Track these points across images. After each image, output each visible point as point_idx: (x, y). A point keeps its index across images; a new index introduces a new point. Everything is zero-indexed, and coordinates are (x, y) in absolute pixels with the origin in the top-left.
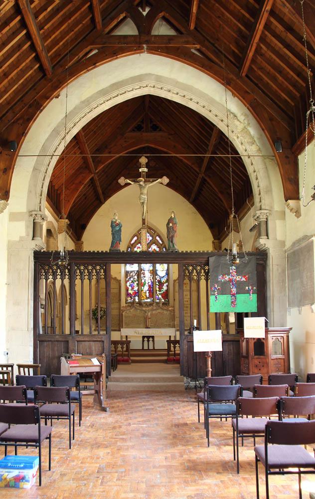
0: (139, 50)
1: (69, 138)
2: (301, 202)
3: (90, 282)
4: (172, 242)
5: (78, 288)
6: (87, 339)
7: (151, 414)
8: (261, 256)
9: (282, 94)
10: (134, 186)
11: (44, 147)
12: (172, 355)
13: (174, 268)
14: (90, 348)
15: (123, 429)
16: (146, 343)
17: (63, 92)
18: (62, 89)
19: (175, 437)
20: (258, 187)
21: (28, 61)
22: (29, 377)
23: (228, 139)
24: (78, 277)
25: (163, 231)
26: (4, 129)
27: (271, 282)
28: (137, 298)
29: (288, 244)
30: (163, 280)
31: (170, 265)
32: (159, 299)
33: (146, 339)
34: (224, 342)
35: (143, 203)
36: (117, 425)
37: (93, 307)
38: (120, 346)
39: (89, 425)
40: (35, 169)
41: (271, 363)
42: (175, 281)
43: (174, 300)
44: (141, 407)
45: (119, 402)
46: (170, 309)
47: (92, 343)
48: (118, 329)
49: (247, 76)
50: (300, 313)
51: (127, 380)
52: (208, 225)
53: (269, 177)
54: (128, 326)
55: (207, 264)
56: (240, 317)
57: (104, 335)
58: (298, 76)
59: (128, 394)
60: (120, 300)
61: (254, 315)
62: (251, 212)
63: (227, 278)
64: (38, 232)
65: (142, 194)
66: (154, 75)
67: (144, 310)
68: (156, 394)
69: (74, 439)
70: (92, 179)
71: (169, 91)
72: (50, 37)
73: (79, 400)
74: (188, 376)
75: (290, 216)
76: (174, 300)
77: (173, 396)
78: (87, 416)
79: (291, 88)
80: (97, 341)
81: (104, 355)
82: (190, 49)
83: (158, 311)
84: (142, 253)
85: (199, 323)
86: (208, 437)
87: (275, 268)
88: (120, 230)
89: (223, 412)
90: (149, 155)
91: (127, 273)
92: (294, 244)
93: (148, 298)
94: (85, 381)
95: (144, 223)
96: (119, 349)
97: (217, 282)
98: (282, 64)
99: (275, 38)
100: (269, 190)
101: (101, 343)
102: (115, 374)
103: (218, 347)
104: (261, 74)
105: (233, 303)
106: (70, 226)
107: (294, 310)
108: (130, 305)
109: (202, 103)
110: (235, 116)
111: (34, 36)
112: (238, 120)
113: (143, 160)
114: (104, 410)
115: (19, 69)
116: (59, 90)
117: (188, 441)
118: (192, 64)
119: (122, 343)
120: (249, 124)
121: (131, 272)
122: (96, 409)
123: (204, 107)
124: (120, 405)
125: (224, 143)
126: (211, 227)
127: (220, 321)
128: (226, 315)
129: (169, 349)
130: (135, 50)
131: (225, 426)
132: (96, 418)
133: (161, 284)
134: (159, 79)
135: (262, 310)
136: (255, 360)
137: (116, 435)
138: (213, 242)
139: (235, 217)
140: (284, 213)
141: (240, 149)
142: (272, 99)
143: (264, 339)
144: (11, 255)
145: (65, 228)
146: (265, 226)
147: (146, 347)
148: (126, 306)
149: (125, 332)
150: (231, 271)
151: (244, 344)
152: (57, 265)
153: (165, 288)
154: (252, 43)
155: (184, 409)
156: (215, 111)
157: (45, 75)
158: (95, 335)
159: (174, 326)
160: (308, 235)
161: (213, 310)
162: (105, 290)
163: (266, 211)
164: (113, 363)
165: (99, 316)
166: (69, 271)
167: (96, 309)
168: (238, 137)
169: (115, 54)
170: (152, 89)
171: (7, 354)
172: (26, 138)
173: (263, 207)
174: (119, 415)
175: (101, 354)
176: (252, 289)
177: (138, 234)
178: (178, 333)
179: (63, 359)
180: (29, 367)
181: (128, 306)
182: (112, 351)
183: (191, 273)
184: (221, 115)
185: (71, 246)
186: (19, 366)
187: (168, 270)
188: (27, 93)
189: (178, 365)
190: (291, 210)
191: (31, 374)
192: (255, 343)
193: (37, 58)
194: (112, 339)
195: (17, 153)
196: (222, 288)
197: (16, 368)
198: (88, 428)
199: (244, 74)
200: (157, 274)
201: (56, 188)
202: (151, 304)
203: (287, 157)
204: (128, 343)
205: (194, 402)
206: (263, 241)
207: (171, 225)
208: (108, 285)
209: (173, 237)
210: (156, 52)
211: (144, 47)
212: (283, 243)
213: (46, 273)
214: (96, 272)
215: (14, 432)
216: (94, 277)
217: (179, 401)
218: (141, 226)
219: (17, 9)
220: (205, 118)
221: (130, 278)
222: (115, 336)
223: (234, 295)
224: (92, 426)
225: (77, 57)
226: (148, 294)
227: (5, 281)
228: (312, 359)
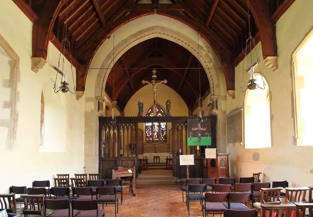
0: (152, 12)
1: (116, 60)
2: (236, 91)
3: (128, 132)
4: (169, 112)
5: (122, 134)
6: (126, 159)
7: (158, 197)
8: (213, 119)
9: (228, 35)
10: (150, 85)
11: (103, 65)
12: (169, 165)
13: (170, 124)
14: (128, 163)
15: (144, 206)
16: (155, 160)
17: (112, 35)
18: (112, 33)
19: (171, 210)
20: (213, 84)
21: (92, 17)
22: (95, 181)
23: (198, 61)
24: (122, 129)
25: (164, 106)
26: (81, 54)
27: (219, 130)
28: (151, 138)
29: (228, 112)
30: (164, 130)
31: (167, 123)
32: (162, 139)
33: (155, 158)
34: (195, 160)
35: (154, 93)
36: (141, 204)
37: (130, 143)
38: (143, 161)
39: (126, 204)
40: (98, 76)
41: (219, 171)
42: (170, 130)
43: (169, 139)
44: (153, 193)
45: (142, 191)
46: (167, 143)
47: (129, 161)
48: (142, 153)
49: (209, 26)
50: (234, 146)
51: (146, 179)
52: (186, 104)
53: (218, 79)
54: (147, 152)
55: (186, 122)
56: (203, 148)
57: (135, 157)
58: (237, 24)
59: (147, 186)
60: (143, 140)
61: (210, 147)
62: (209, 96)
63: (196, 129)
64: (101, 107)
65: (153, 88)
66: (160, 26)
67: (154, 144)
68: (161, 186)
69: (118, 213)
70: (129, 82)
71: (168, 35)
72: (104, 3)
73: (121, 191)
74: (177, 176)
75: (229, 98)
76: (169, 139)
77: (170, 187)
78: (125, 199)
79: (233, 32)
80: (131, 160)
81: (134, 167)
82: (179, 11)
83: (161, 145)
84: (154, 117)
85: (182, 151)
86: (188, 210)
87: (221, 124)
88: (143, 106)
89: (196, 198)
90: (157, 69)
91: (146, 127)
92: (231, 112)
93: (157, 138)
94: (125, 180)
95: (155, 103)
96: (143, 163)
97: (191, 131)
98: (229, 18)
99: (226, 3)
100: (218, 86)
101: (133, 161)
102: (140, 176)
103: (192, 163)
104: (218, 25)
105: (199, 141)
106: (118, 104)
107: (231, 145)
108: (148, 142)
109: (185, 41)
110: (202, 48)
111: (94, 2)
112: (203, 50)
113: (154, 71)
114: (134, 195)
115: (87, 21)
116: (109, 34)
117: (178, 213)
118: (180, 20)
119: (144, 160)
120: (209, 52)
121: (148, 126)
122: (130, 195)
123: (186, 43)
124: (143, 192)
125: (196, 62)
126: (188, 104)
127: (192, 150)
128: (195, 147)
129: (167, 163)
130: (150, 12)
131: (197, 204)
132: (130, 200)
133: (163, 132)
134: (163, 28)
135: (214, 145)
136: (211, 169)
137: (140, 210)
138: (188, 112)
139: (201, 99)
140: (226, 97)
141: (204, 65)
142: (222, 38)
143: (215, 159)
144: (87, 119)
145: (115, 105)
146: (216, 103)
147: (155, 162)
148: (146, 143)
149: (146, 155)
150: (198, 126)
151: (205, 161)
152: (111, 123)
153: (165, 133)
154: (213, 6)
155: (175, 194)
156: (191, 46)
157: (102, 25)
158: (130, 157)
159: (169, 152)
160: (239, 107)
161: (189, 144)
162: (135, 135)
163: (216, 96)
164: (139, 170)
165: (133, 148)
166: (117, 126)
167: (131, 144)
168: (203, 59)
169: (139, 14)
170: (159, 34)
171: (85, 168)
172: (93, 59)
173: (215, 94)
174: (142, 198)
175: (134, 166)
176: (209, 134)
177: (152, 108)
178: (171, 155)
179: (113, 170)
180: (95, 175)
181: (147, 142)
182: (139, 164)
183: (178, 127)
184: (194, 48)
185: (118, 114)
186: (90, 175)
187: (166, 125)
188: (92, 34)
189: (172, 171)
190: (230, 95)
191: (97, 179)
192: (211, 161)
193: (97, 16)
194: (139, 158)
195: (88, 67)
196: (194, 134)
197: (88, 176)
198: (126, 206)
199: (207, 25)
200: (161, 127)
201: (110, 85)
202: (158, 141)
203: (229, 68)
204: (147, 160)
205: (180, 190)
206: (215, 111)
207: (168, 103)
208: (136, 133)
209: (169, 109)
210: (161, 14)
211: (154, 11)
212: (225, 112)
213: (105, 128)
214: (131, 126)
215: (83, 214)
216: (130, 129)
217: (173, 190)
218: (153, 104)
219: (91, 2)
220: (186, 49)
221: (148, 129)
222: (141, 157)
223: (199, 137)
224: (128, 205)
225: (119, 16)
226: (156, 137)
227: (84, 132)
228: (241, 169)
